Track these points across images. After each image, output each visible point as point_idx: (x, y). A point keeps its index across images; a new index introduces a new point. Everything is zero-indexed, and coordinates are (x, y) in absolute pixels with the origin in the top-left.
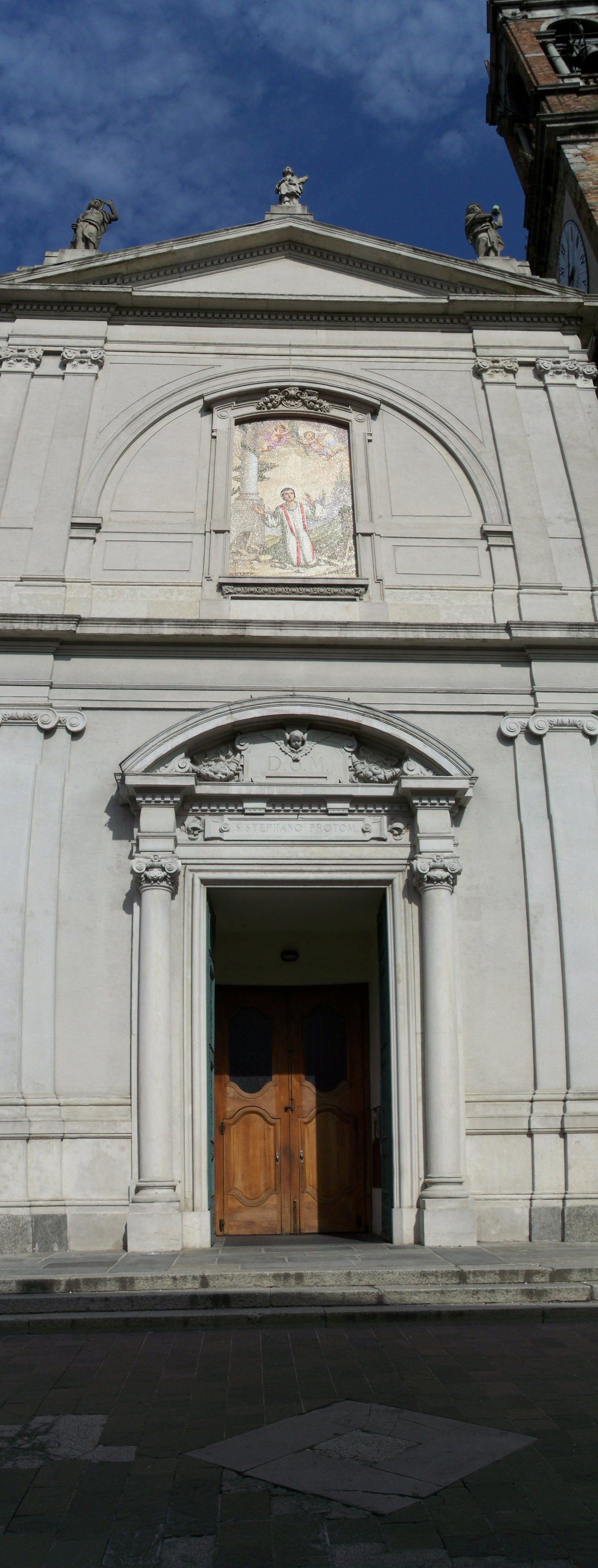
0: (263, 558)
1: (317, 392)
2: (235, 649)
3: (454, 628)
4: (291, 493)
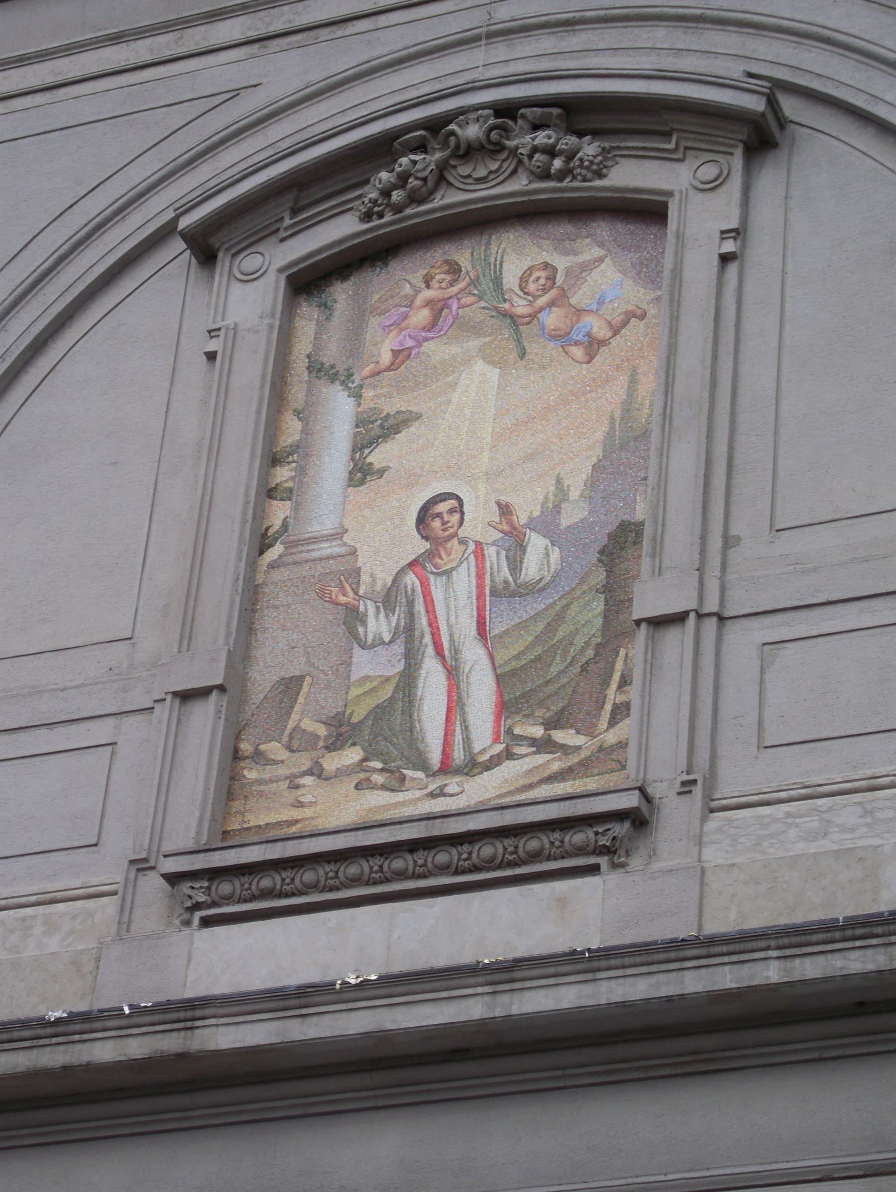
0: (332, 762)
1: (555, 111)
2: (181, 1100)
3: (879, 930)
4: (451, 511)
